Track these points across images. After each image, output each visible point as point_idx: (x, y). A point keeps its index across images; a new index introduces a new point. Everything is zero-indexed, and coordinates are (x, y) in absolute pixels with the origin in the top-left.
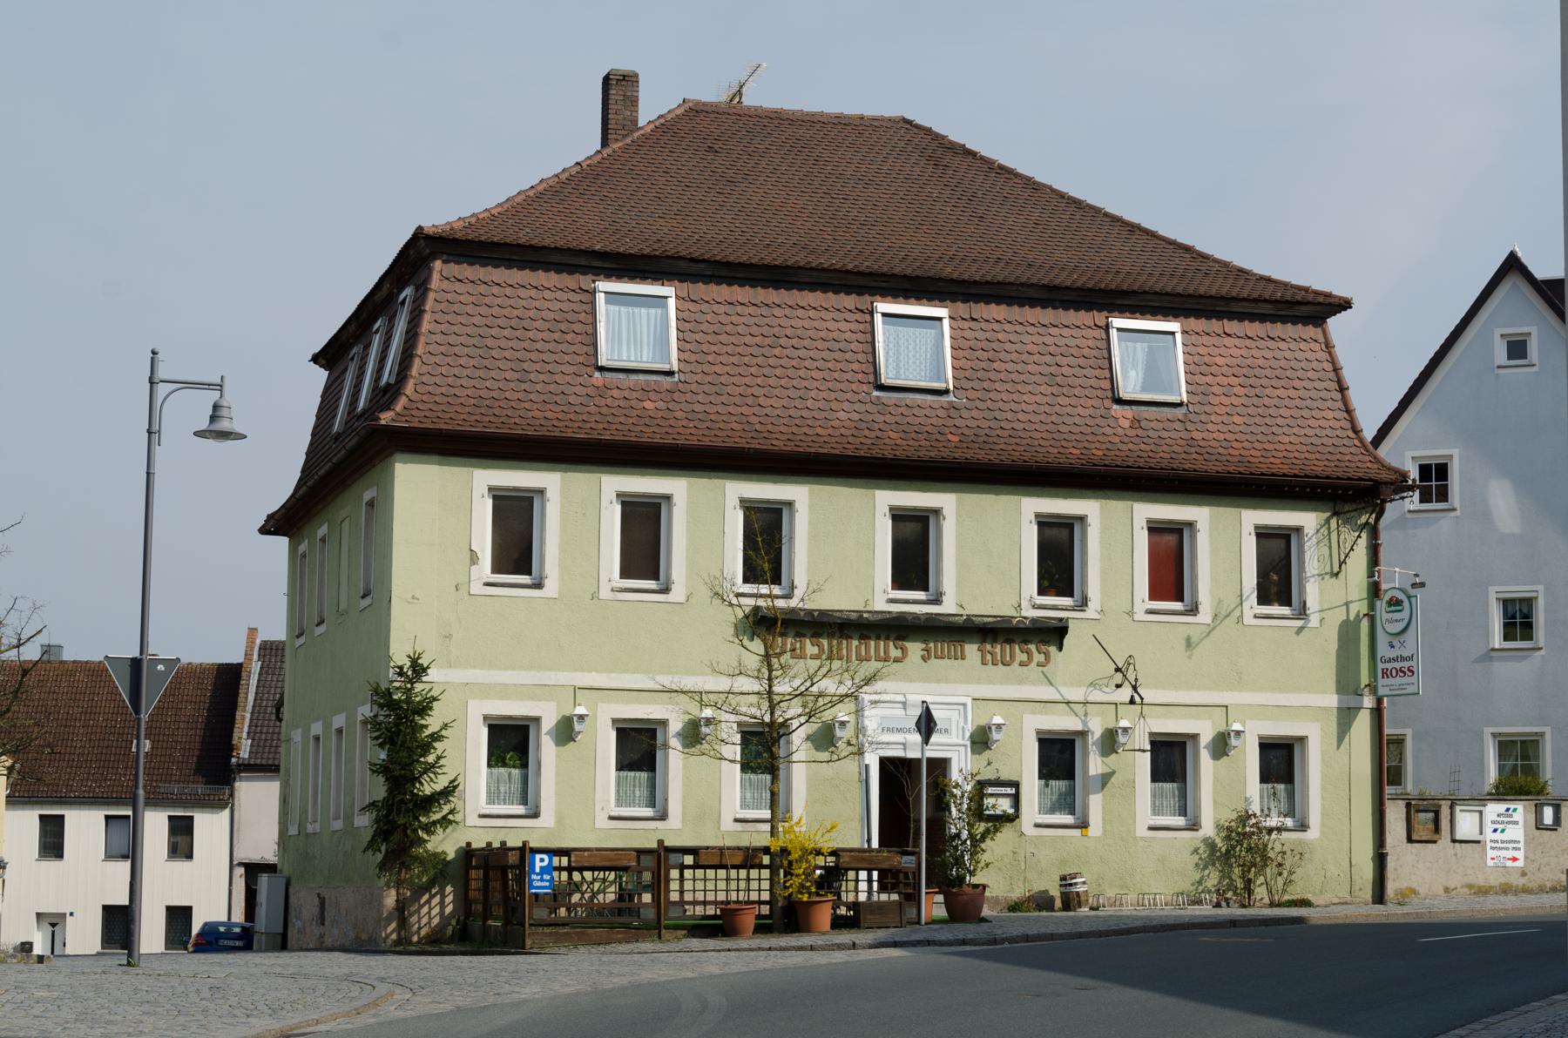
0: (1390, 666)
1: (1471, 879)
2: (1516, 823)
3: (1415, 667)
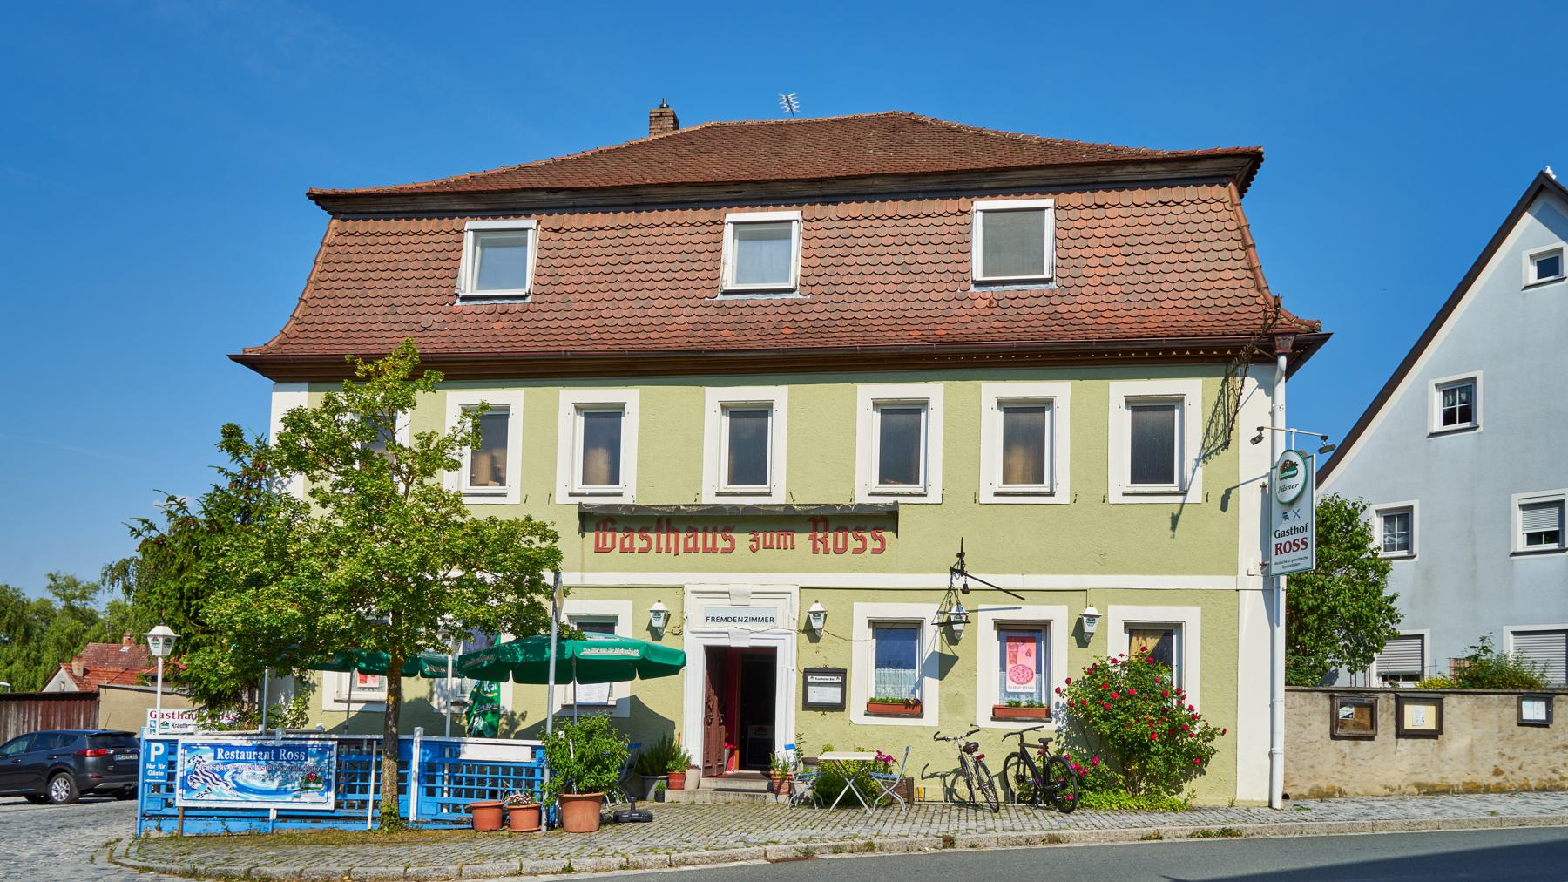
0: (1283, 540)
3: (1309, 539)
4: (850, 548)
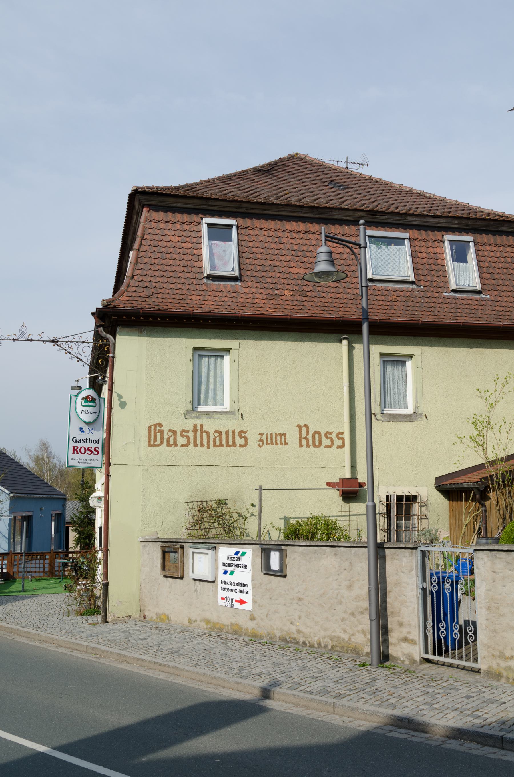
0: (80, 445)
1: (208, 615)
2: (244, 566)
4: (323, 444)
